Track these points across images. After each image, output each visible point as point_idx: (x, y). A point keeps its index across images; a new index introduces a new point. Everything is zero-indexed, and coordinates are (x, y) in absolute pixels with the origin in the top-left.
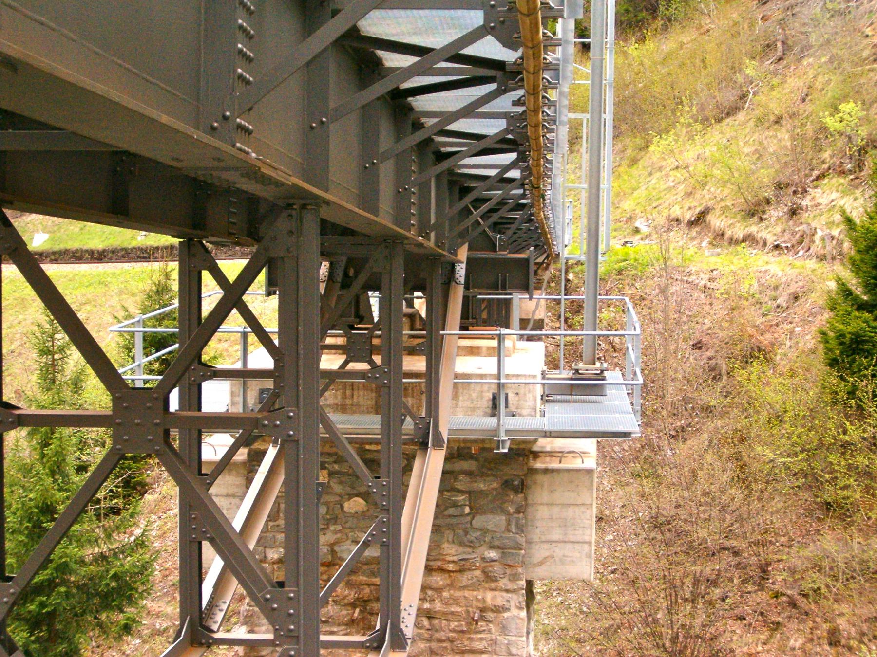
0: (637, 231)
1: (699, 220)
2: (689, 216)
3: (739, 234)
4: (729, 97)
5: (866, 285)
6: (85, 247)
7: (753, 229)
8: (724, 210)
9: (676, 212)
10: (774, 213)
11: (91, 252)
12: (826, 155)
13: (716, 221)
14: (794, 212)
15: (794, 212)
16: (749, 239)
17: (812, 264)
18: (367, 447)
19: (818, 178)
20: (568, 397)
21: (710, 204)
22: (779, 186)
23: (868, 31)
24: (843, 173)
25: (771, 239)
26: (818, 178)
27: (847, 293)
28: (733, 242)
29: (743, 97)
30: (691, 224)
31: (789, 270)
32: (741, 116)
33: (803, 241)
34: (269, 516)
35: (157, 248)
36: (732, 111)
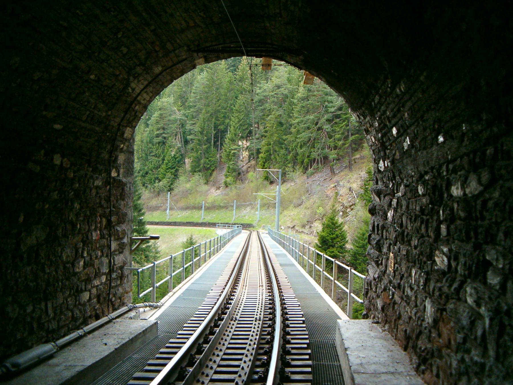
0: (282, 229)
1: (294, 227)
2: (291, 226)
3: (301, 231)
4: (300, 202)
5: (320, 244)
6: (154, 221)
7: (303, 230)
8: (298, 226)
9: (289, 225)
10: (307, 227)
11: (155, 222)
12: (317, 216)
13: (297, 228)
14: (310, 227)
15: (310, 227)
16: (302, 232)
17: (313, 237)
18: (386, 166)
19: (315, 220)
20: (80, 332)
21: (296, 224)
22: (308, 222)
23: (326, 191)
24: (319, 220)
25: (306, 232)
26: (315, 220)
27: (317, 245)
28: (299, 232)
29: (302, 202)
30: (292, 228)
31: (309, 239)
32: (302, 206)
33: (312, 233)
34: (316, 281)
35: (172, 222)
36: (300, 205)
